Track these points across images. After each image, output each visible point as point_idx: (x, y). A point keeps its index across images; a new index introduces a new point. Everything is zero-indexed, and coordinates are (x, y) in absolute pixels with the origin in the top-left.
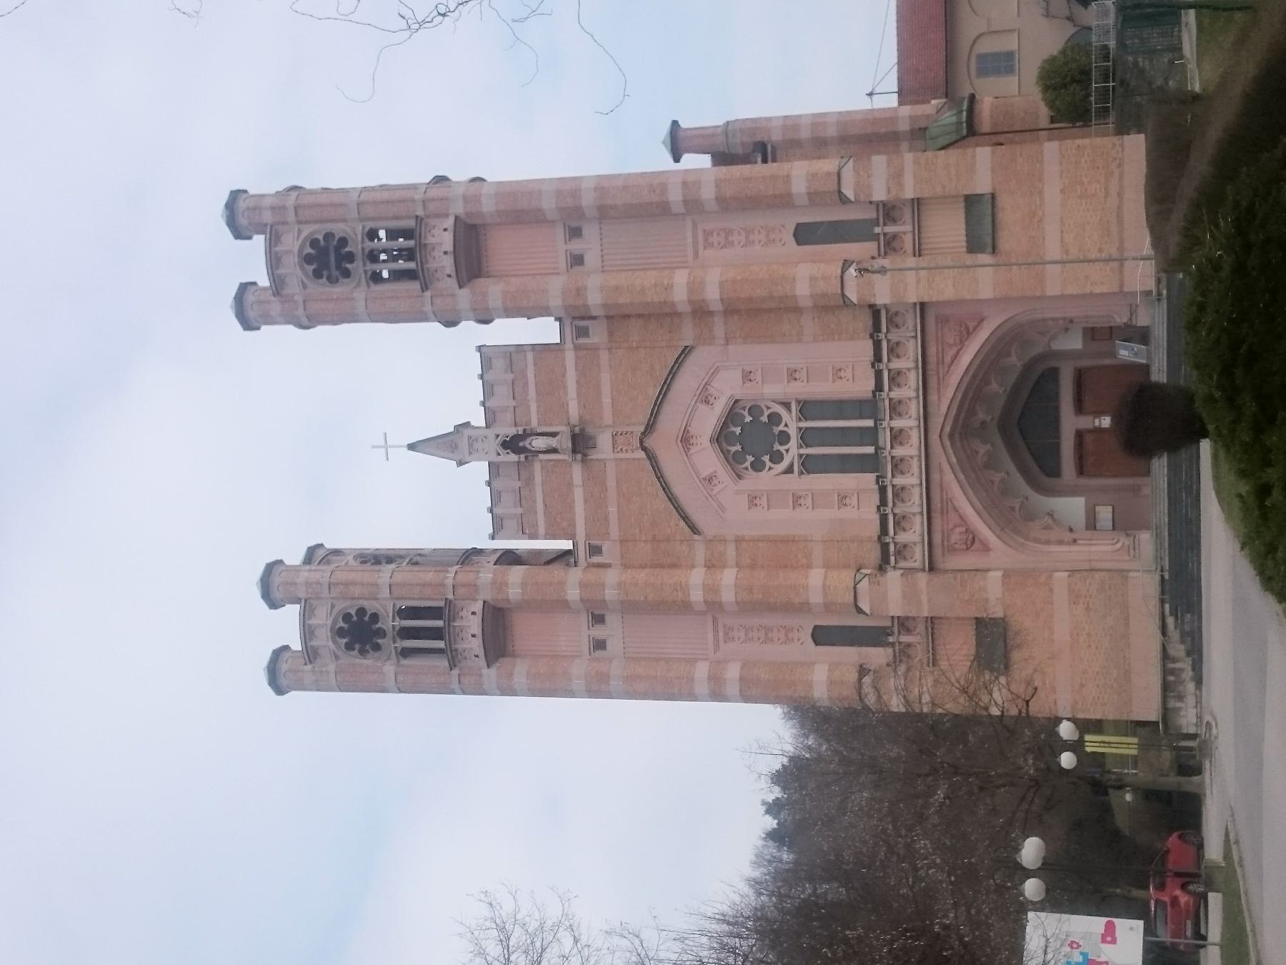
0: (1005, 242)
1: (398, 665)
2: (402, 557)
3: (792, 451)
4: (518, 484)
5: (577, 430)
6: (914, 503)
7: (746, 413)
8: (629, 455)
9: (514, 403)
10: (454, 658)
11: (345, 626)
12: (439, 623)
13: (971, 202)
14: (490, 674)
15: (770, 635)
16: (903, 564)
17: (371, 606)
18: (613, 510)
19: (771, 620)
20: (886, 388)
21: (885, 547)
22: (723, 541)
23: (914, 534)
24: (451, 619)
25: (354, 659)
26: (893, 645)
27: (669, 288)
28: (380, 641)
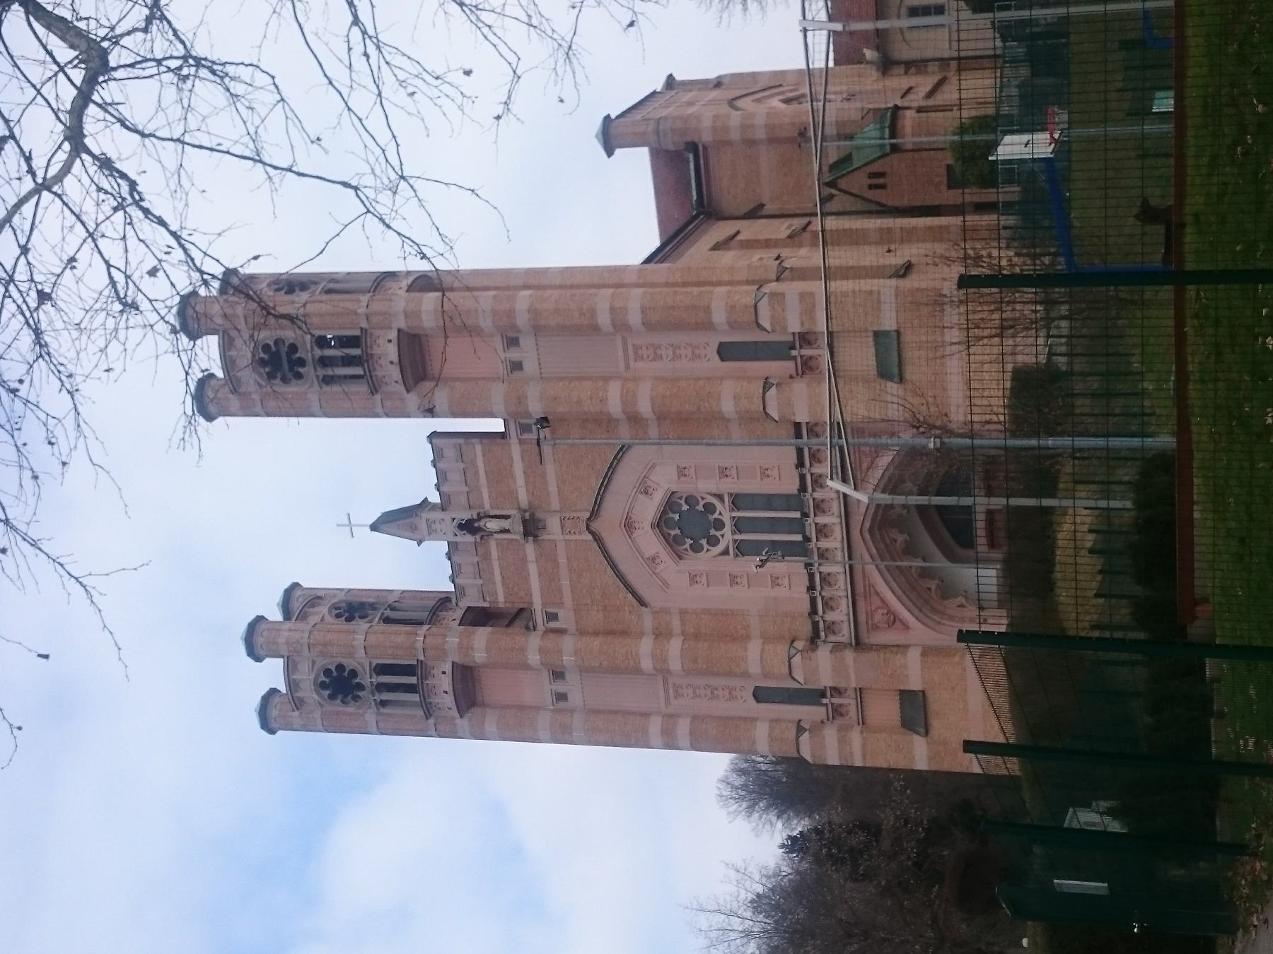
0: (911, 373)
1: (379, 714)
2: (373, 607)
3: (727, 536)
4: (477, 559)
5: (527, 516)
6: (840, 588)
7: (683, 502)
8: (577, 537)
9: (467, 489)
10: (429, 710)
11: (266, 356)
12: (413, 680)
13: (879, 337)
14: (462, 723)
15: (678, 352)
16: (832, 638)
17: (349, 663)
18: (565, 583)
19: (680, 338)
20: (810, 489)
21: (815, 625)
22: (666, 611)
23: (840, 614)
24: (424, 677)
25: (337, 706)
26: (794, 358)
27: (603, 400)
28: (301, 370)
